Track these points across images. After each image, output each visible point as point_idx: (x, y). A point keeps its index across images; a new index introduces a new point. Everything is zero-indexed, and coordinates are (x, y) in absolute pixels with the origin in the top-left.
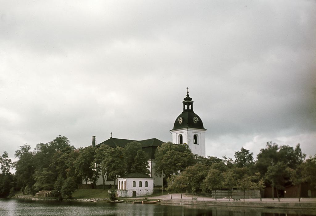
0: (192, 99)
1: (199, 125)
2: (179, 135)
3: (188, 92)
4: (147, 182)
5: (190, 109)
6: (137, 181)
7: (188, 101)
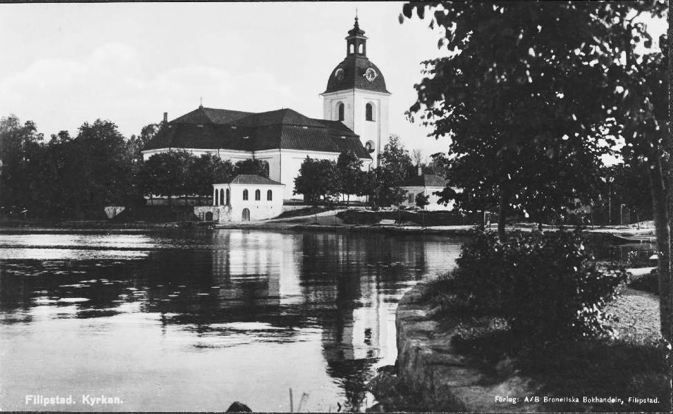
0: (364, 33)
2: (338, 103)
3: (356, 19)
5: (361, 51)
6: (252, 189)
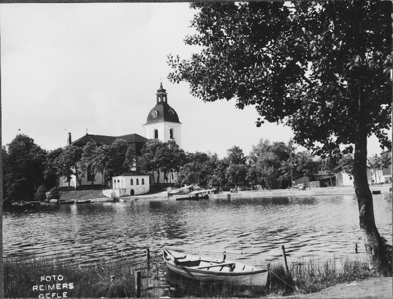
0: (166, 90)
3: (161, 84)
4: (143, 179)
5: (164, 101)
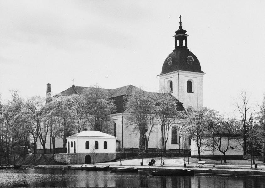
0: (186, 31)
1: (193, 65)
2: (168, 81)
3: (181, 23)
5: (184, 45)
7: (181, 35)
